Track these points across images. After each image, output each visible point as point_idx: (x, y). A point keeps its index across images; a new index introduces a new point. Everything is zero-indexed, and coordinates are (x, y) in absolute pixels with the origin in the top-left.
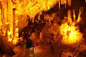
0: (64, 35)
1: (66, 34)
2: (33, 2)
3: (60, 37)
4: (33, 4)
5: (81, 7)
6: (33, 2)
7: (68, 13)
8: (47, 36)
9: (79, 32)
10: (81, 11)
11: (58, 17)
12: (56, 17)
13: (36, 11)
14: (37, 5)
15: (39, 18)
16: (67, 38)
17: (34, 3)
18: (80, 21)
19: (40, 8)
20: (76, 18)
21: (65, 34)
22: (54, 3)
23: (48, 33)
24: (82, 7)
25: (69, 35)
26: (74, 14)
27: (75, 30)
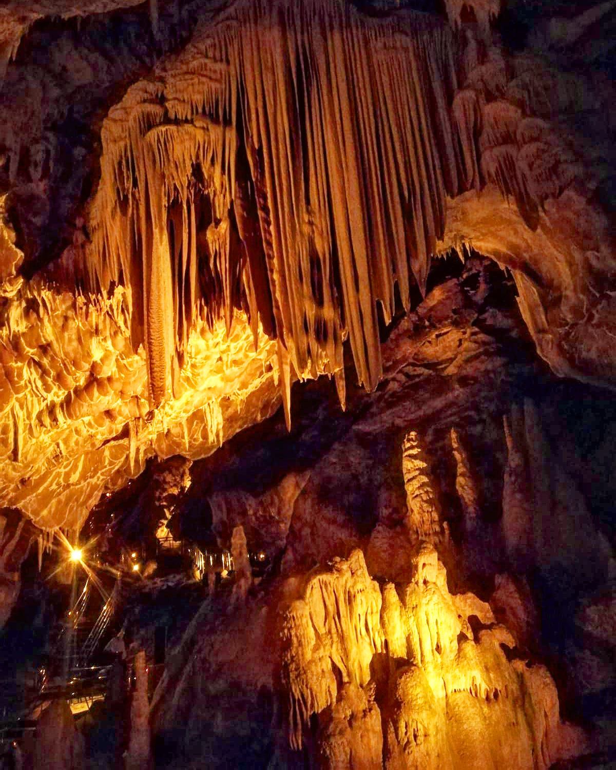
0: (343, 713)
1: (359, 698)
2: (59, 378)
3: (297, 741)
4: (57, 395)
5: (521, 405)
6: (59, 378)
7: (407, 465)
8: (207, 728)
9: (511, 654)
10: (510, 426)
11: (328, 512)
12: (307, 508)
13: (94, 460)
14: (102, 400)
15: (162, 532)
16: (386, 752)
17: (71, 383)
18: (205, 235)
19: (125, 433)
20: (480, 501)
21: (352, 690)
22: (256, 383)
23: (215, 687)
24: (529, 406)
25: (398, 705)
26: (461, 469)
27: (462, 638)
